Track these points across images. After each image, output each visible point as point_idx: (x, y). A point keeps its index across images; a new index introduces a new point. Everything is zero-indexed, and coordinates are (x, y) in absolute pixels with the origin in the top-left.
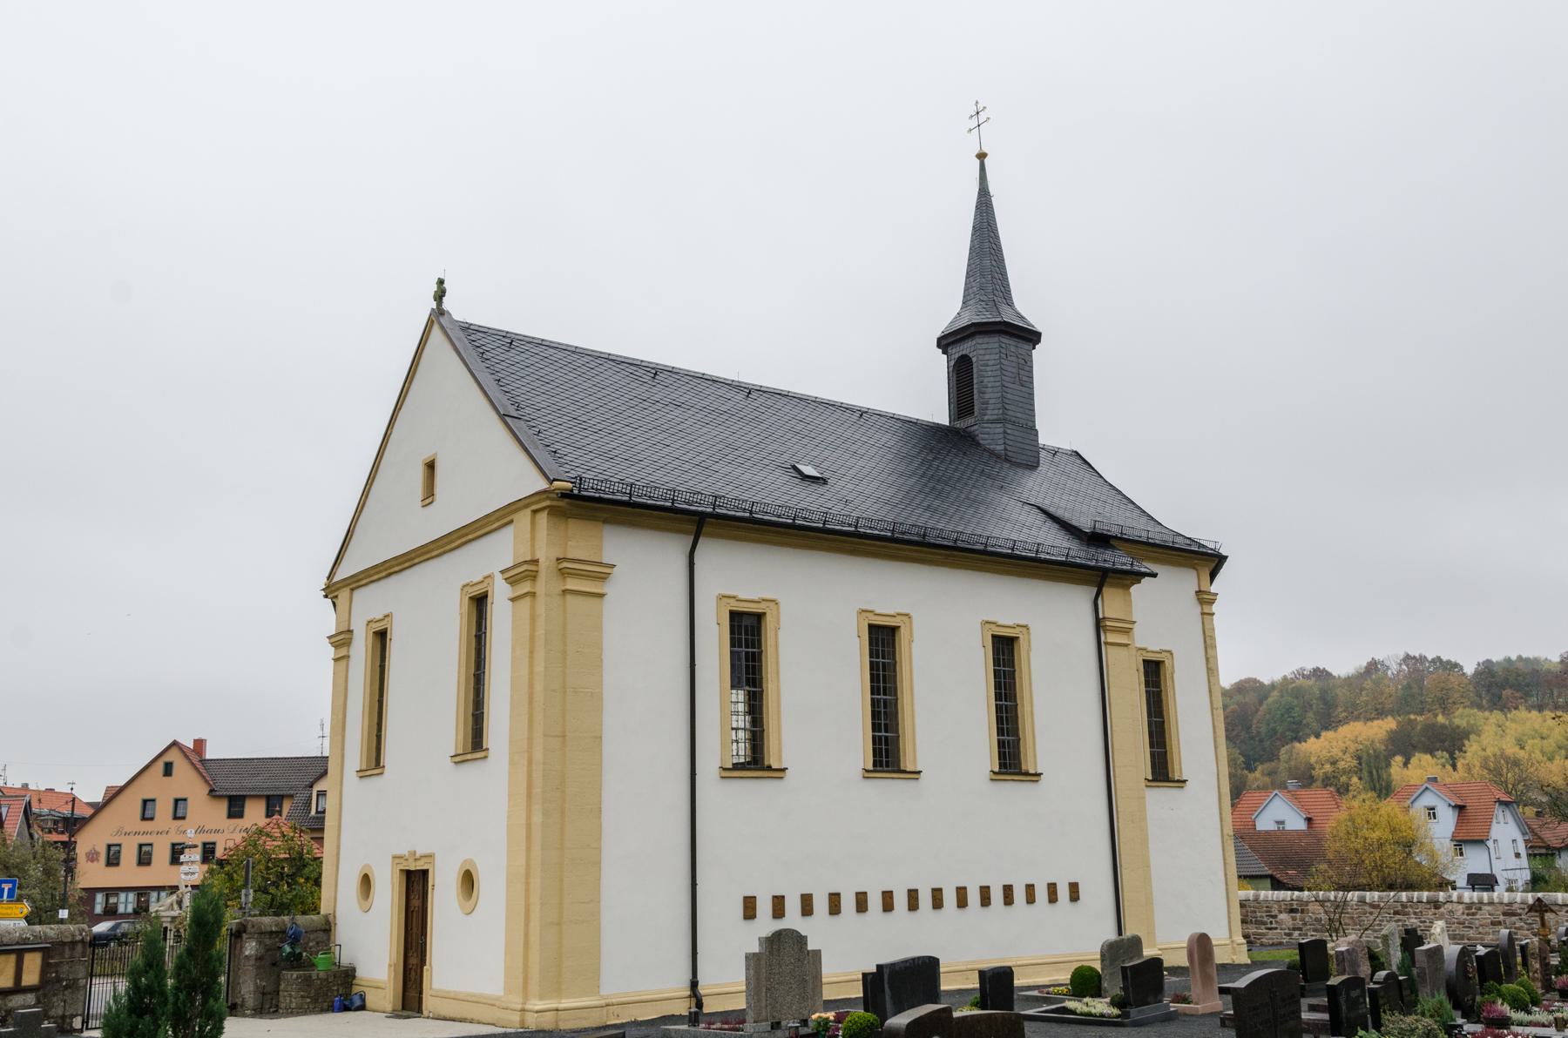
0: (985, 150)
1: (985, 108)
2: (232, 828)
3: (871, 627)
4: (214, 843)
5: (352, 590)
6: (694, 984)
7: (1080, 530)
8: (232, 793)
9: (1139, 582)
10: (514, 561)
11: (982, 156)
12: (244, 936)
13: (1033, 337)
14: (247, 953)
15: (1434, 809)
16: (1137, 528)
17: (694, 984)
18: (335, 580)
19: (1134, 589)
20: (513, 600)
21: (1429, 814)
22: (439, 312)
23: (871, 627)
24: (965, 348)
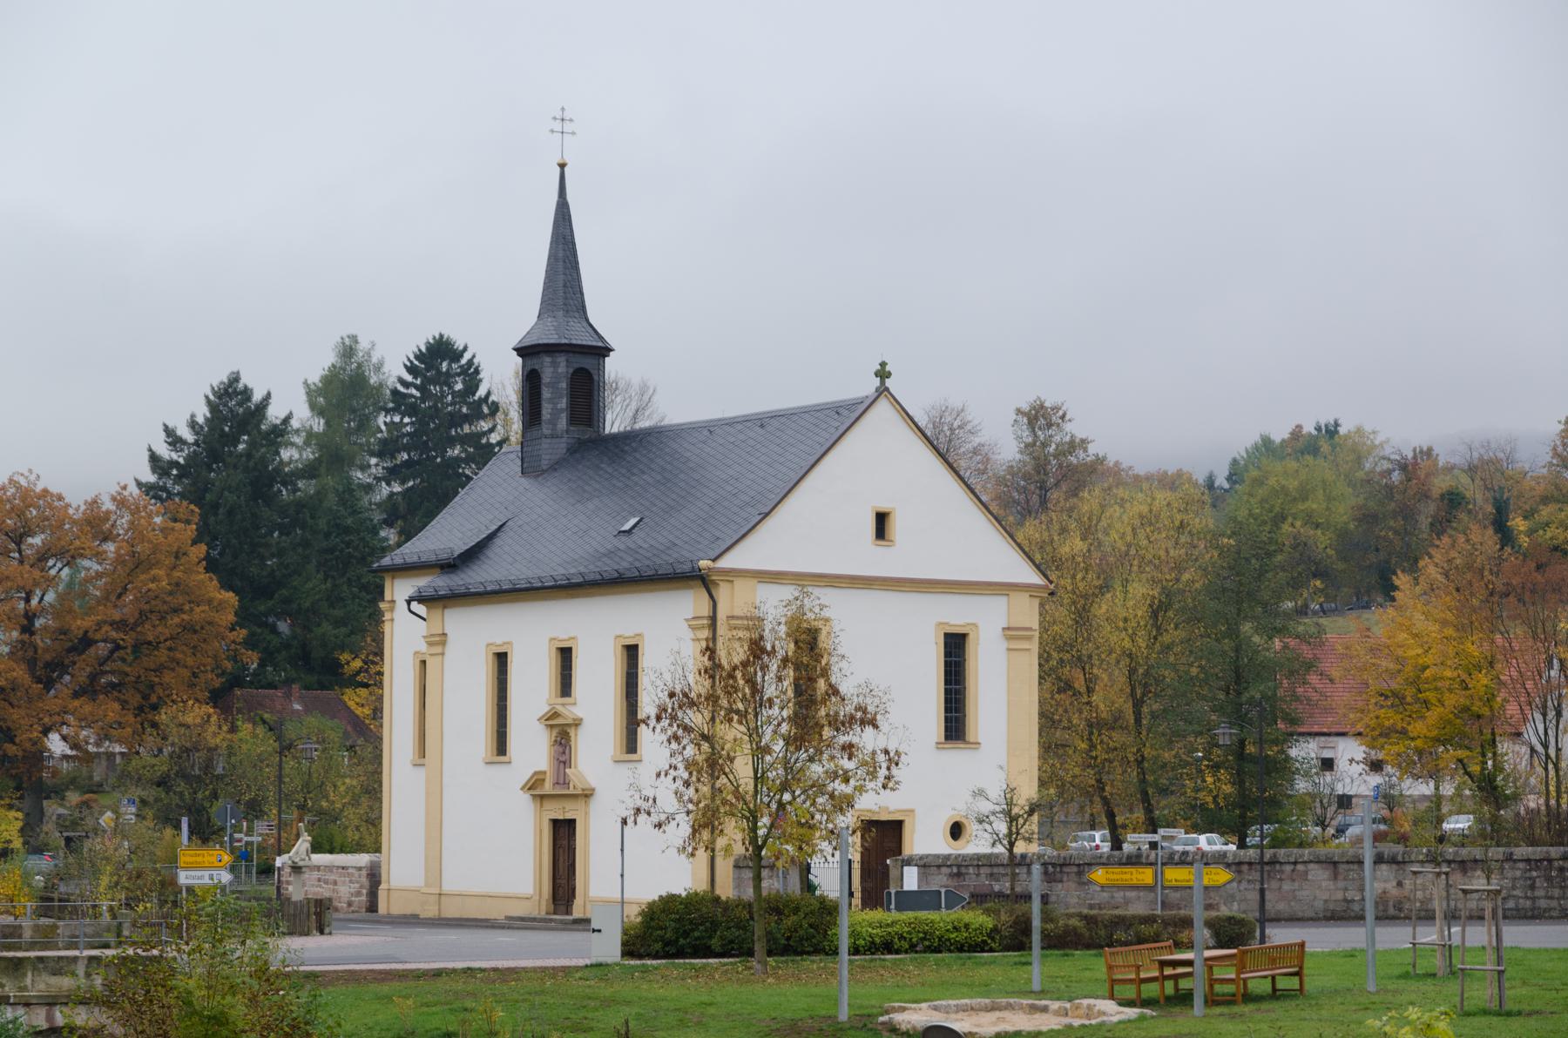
11: (562, 166)
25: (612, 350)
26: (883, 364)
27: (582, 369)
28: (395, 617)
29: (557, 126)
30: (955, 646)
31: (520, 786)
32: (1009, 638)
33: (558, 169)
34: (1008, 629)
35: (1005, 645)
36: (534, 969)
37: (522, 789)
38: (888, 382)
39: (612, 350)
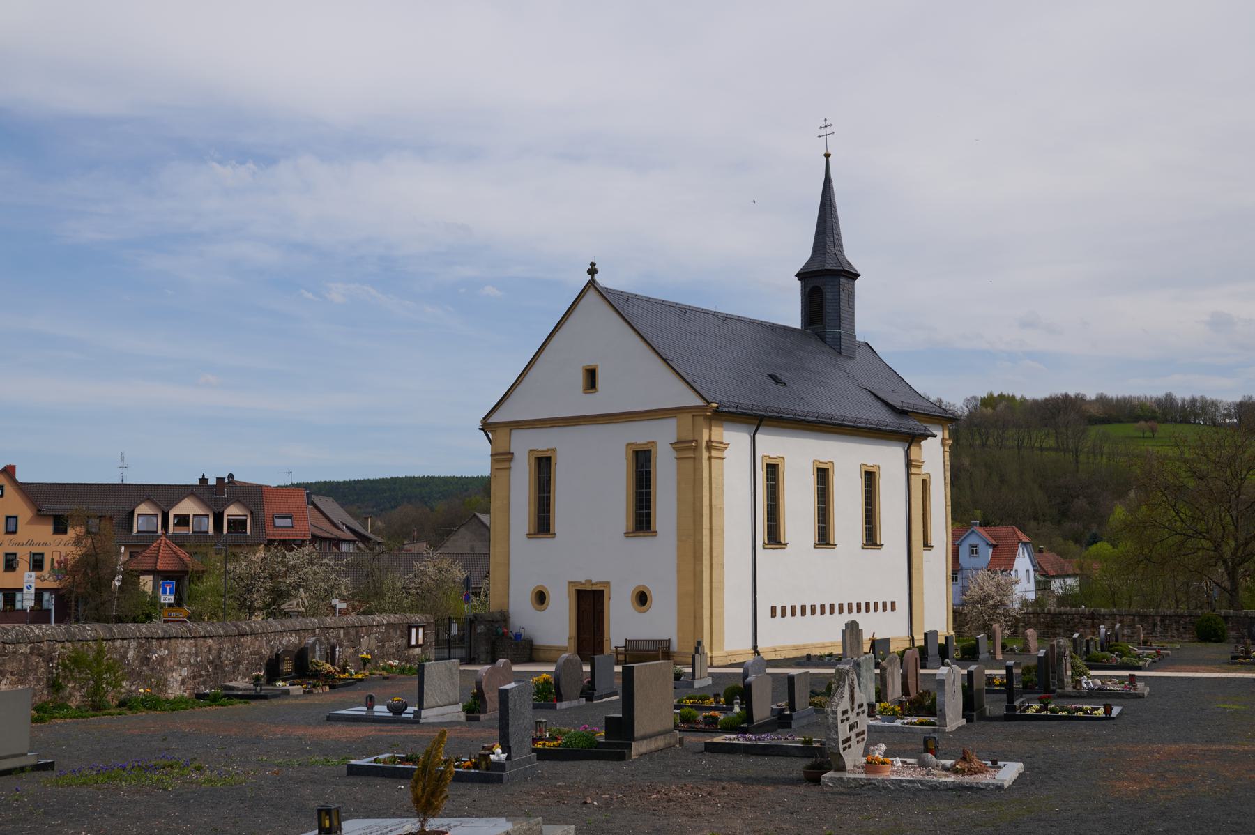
0: (830, 152)
1: (833, 133)
2: (57, 542)
3: (818, 469)
4: (42, 555)
5: (511, 430)
6: (755, 648)
7: (896, 408)
8: (57, 514)
9: (926, 439)
10: (678, 439)
11: (827, 156)
12: (476, 622)
13: (855, 276)
14: (479, 631)
15: (976, 547)
16: (920, 406)
17: (755, 648)
18: (488, 422)
19: (924, 443)
20: (677, 459)
21: (972, 550)
22: (592, 284)
23: (818, 469)
24: (818, 282)
25: (859, 275)
26: (593, 264)
27: (817, 287)
28: (512, 466)
29: (823, 132)
30: (642, 462)
31: (571, 580)
32: (676, 449)
33: (825, 158)
34: (496, 454)
35: (674, 454)
36: (850, 640)
37: (570, 583)
38: (596, 277)
39: (860, 275)
